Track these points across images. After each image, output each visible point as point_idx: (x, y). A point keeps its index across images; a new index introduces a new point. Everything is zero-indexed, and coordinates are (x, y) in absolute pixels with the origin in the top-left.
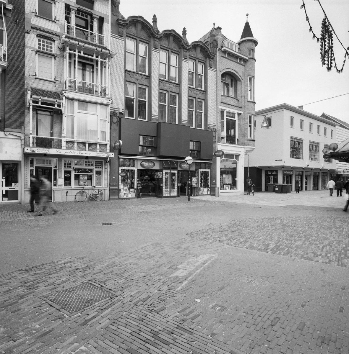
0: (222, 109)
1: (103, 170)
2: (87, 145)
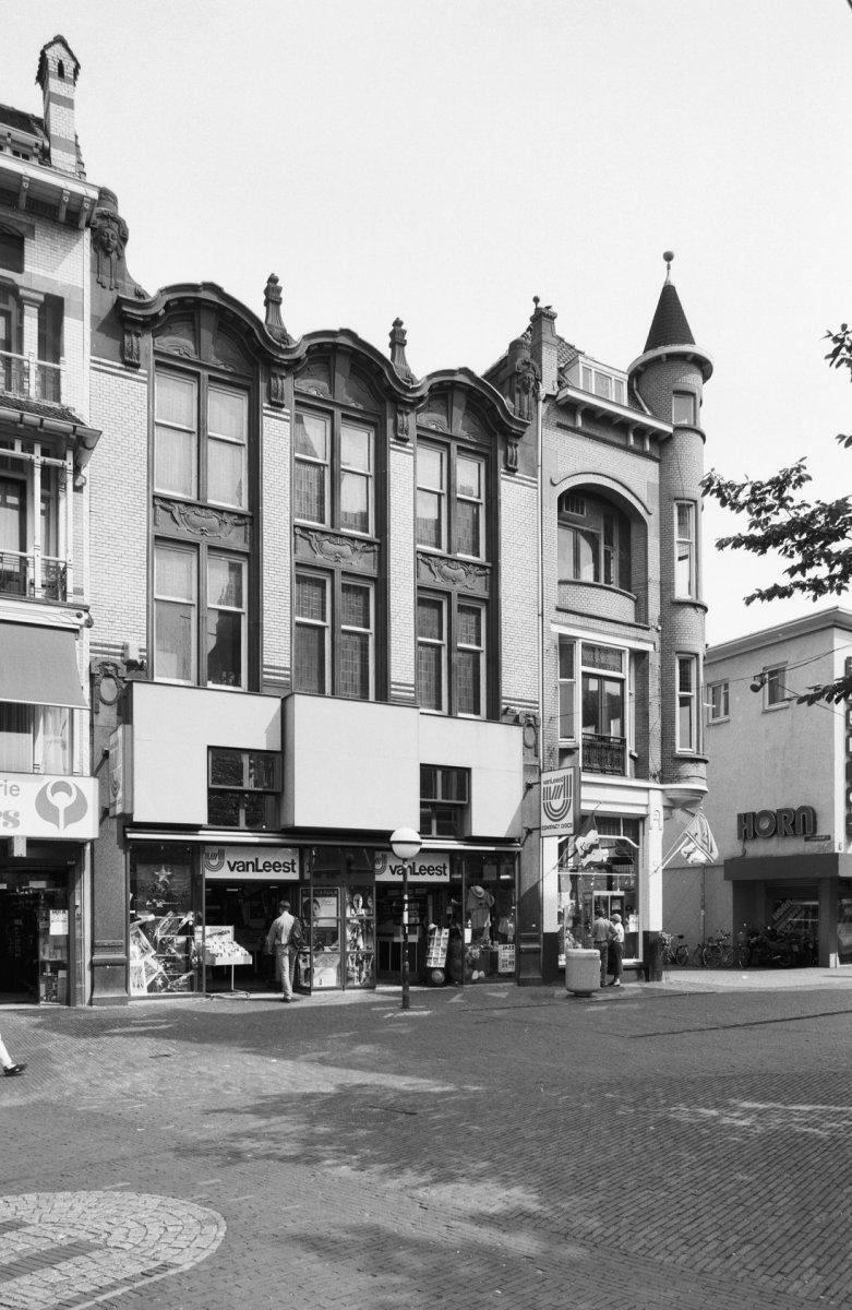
0: (561, 637)
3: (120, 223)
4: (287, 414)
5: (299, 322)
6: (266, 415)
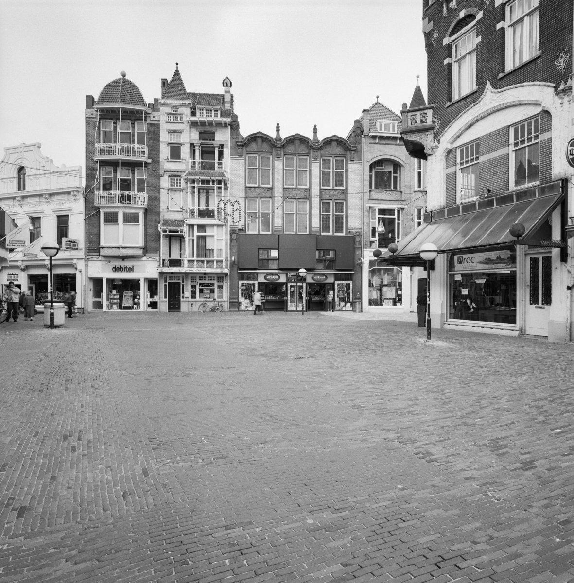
1: (224, 284)
2: (205, 263)
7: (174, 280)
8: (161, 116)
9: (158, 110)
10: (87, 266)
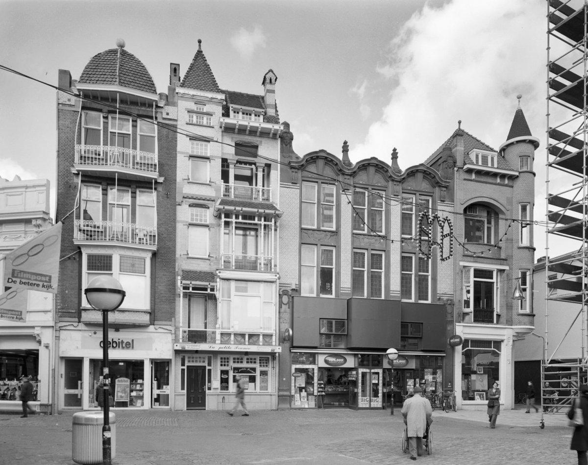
2: (247, 337)
3: (291, 134)
4: (350, 192)
5: (355, 157)
6: (439, 205)
7: (196, 361)
8: (179, 112)
9: (174, 104)
10: (58, 338)
